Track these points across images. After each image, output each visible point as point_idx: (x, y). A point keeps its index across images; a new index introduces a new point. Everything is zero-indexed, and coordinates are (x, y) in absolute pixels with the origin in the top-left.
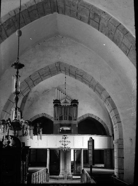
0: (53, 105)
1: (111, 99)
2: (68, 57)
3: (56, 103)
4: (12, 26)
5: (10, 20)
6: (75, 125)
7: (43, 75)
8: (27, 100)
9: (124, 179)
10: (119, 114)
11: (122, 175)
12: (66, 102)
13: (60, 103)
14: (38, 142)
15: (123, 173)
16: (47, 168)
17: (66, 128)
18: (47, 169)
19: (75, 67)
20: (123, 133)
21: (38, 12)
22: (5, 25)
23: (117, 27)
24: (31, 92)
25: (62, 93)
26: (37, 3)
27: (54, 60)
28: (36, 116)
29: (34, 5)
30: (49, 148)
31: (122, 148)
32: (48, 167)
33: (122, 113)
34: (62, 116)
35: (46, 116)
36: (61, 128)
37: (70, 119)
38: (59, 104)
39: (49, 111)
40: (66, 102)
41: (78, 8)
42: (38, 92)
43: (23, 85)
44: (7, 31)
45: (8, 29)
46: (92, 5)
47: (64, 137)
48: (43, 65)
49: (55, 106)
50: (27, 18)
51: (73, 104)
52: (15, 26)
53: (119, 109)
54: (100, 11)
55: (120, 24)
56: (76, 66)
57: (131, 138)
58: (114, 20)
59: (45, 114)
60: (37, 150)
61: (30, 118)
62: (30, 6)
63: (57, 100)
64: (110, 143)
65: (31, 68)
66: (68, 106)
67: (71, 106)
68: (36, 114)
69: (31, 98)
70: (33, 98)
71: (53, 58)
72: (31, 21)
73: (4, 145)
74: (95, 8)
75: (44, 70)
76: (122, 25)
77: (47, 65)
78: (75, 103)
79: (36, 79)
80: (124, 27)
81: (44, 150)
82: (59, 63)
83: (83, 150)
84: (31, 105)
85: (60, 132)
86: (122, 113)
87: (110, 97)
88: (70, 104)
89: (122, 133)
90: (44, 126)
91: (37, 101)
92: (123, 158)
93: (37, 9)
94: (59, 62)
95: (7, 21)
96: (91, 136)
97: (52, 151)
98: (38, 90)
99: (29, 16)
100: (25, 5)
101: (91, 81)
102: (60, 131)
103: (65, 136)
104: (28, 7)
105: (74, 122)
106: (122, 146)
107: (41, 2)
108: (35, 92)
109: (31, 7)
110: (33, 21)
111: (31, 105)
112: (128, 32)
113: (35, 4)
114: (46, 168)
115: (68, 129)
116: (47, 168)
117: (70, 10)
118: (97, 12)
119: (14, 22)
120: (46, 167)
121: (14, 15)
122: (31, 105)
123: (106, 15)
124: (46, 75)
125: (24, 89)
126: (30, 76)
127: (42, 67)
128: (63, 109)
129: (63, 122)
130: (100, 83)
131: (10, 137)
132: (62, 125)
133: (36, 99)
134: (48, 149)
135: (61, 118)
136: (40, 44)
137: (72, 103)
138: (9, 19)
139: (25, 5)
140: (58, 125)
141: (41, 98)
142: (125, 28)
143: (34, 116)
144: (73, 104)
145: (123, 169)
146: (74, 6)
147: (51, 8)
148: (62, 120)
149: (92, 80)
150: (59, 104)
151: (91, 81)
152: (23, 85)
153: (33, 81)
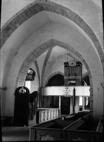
0: (64, 65)
1: (86, 62)
2: (57, 36)
3: (78, 64)
4: (17, 22)
5: (15, 19)
6: (79, 79)
7: (43, 48)
8: (47, 63)
9: (93, 115)
10: (90, 72)
11: (92, 112)
12: (72, 64)
13: (68, 64)
14: (54, 91)
15: (92, 112)
16: (59, 109)
17: (72, 82)
18: (59, 109)
19: (62, 42)
20: (93, 84)
21: (32, 12)
22: (13, 23)
23: (76, 17)
24: (50, 58)
25: (70, 56)
26: (29, 8)
27: (49, 39)
28: (54, 74)
29: (28, 9)
30: (60, 96)
31: (92, 94)
32: (60, 108)
33: (92, 71)
34: (70, 73)
35: (60, 74)
36: (69, 82)
37: (76, 75)
38: (68, 65)
39: (61, 70)
40: (72, 64)
41: (53, 7)
42: (55, 57)
43: (31, 55)
44: (15, 26)
45: (15, 24)
46: (61, 5)
47: (66, 88)
48: (42, 42)
49: (65, 66)
50: (26, 17)
51: (77, 65)
52: (19, 22)
53: (90, 68)
54: (65, 8)
55: (78, 15)
56: (63, 42)
57: (99, 88)
58: (74, 13)
59: (59, 72)
60: (53, 97)
61: (50, 75)
62: (25, 10)
63: (66, 62)
64: (91, 90)
65: (35, 44)
66: (74, 66)
67: (76, 66)
68: (53, 73)
69: (50, 62)
70: (52, 62)
71: (47, 37)
72: (30, 18)
73: (20, 93)
74: (63, 7)
75: (43, 45)
76: (79, 16)
77: (44, 42)
78: (79, 64)
79: (39, 51)
80: (80, 16)
81: (57, 97)
82: (52, 40)
83: (87, 98)
84: (51, 66)
85: (68, 84)
86: (92, 71)
87: (84, 60)
88: (75, 65)
89: (93, 84)
90: (57, 80)
91: (54, 63)
92: (93, 101)
93: (30, 11)
94: (52, 39)
95: (13, 20)
96: (74, 87)
97: (62, 97)
98: (54, 56)
99: (27, 15)
100: (23, 9)
101: (72, 50)
102: (69, 83)
103: (67, 87)
104: (24, 11)
105: (79, 77)
106: (92, 93)
107: (31, 7)
108: (52, 58)
109: (26, 10)
110: (31, 17)
111: (50, 67)
112: (82, 20)
113: (28, 8)
114: (58, 109)
115: (74, 82)
116: (59, 109)
117: (51, 9)
118: (63, 9)
119: (18, 20)
120: (59, 108)
121: (17, 16)
122: (51, 66)
123: (69, 10)
124: (45, 48)
125: (32, 58)
126: (35, 50)
127: (42, 44)
128: (71, 68)
129: (71, 77)
130: (78, 52)
131: (23, 88)
132: (70, 80)
133: (54, 62)
134: (60, 96)
135: (69, 75)
136: (41, 29)
137: (76, 64)
138: (14, 19)
139: (23, 9)
140: (67, 80)
141: (57, 61)
142: (80, 18)
143: (52, 74)
144: (77, 65)
145: (93, 109)
146: (51, 6)
147: (39, 8)
148: (70, 76)
149: (73, 50)
150: (68, 65)
151: (72, 50)
152: (31, 55)
153: (38, 53)
